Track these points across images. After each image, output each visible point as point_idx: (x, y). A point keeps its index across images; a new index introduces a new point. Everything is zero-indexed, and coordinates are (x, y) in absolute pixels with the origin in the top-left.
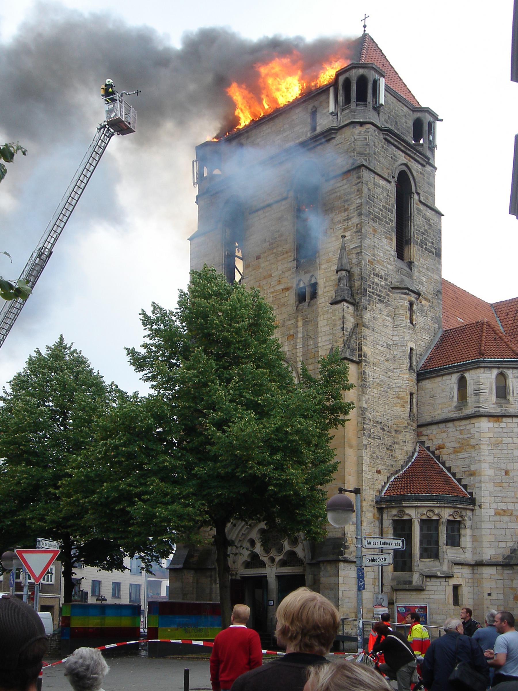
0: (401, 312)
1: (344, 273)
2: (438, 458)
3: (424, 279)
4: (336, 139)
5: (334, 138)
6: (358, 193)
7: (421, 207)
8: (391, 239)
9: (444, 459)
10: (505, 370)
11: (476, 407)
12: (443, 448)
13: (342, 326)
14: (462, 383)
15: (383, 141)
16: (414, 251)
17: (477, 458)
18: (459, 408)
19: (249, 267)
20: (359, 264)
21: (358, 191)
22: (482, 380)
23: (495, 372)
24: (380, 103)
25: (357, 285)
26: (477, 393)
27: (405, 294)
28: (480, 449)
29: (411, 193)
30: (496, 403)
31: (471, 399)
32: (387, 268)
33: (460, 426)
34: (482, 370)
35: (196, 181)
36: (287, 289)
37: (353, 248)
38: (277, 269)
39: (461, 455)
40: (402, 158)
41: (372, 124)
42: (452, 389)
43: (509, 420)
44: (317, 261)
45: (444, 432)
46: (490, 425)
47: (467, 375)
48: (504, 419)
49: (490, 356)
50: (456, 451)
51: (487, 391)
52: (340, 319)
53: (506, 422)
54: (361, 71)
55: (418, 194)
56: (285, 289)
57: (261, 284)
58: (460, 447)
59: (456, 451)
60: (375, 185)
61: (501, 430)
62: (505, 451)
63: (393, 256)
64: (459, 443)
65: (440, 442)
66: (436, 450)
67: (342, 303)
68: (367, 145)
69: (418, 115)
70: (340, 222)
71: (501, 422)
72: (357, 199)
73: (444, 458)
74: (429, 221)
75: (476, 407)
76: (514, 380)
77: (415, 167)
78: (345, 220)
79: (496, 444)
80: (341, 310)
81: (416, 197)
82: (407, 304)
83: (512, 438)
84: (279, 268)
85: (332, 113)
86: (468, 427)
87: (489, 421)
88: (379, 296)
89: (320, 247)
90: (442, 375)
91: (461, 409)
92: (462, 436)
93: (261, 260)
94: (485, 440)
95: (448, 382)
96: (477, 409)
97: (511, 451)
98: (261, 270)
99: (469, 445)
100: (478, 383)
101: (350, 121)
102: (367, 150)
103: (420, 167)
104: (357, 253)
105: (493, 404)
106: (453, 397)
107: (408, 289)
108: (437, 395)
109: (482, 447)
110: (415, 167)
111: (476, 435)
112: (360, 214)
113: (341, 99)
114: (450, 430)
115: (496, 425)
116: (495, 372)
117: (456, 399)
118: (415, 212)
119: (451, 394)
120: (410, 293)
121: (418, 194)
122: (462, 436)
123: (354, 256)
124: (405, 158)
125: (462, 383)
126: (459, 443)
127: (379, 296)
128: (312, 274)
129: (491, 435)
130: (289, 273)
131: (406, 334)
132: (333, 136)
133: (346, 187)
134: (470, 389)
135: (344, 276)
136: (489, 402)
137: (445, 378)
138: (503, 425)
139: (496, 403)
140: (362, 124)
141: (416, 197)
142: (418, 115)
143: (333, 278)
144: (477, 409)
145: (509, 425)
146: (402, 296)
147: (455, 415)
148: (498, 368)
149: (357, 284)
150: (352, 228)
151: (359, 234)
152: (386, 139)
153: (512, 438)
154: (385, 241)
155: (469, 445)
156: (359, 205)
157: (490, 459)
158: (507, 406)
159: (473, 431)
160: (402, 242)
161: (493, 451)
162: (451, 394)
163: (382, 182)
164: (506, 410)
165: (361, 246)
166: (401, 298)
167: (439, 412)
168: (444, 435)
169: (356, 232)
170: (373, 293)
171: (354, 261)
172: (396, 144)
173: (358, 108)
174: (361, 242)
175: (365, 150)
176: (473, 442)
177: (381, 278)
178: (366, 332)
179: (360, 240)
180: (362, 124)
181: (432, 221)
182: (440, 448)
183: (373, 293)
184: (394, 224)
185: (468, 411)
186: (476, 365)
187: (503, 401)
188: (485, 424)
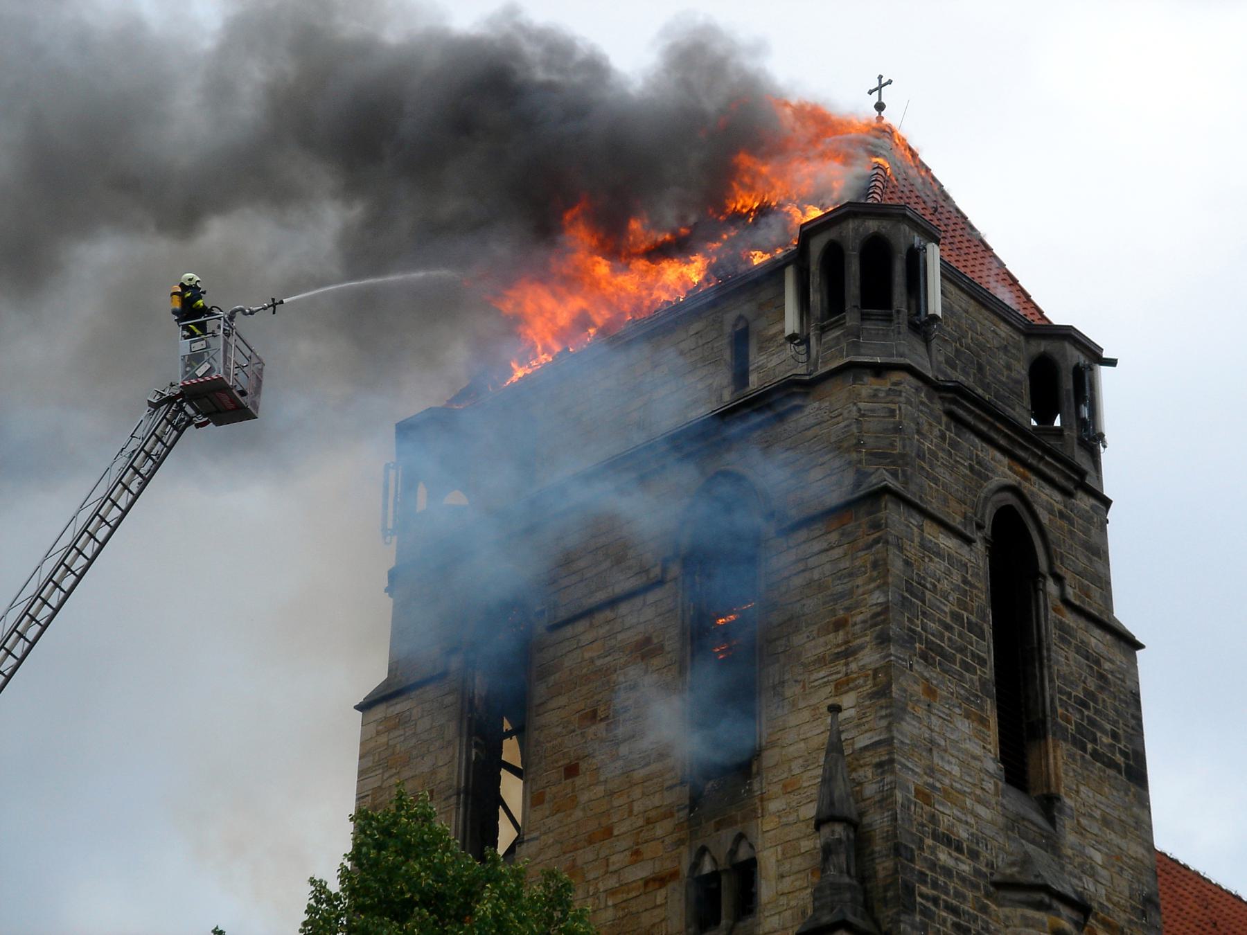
1: (839, 830)
3: (1098, 858)
4: (807, 411)
5: (798, 408)
6: (875, 574)
7: (1070, 619)
8: (983, 721)
15: (944, 419)
16: (1060, 761)
19: (542, 802)
21: (875, 565)
24: (930, 312)
25: (881, 874)
27: (1039, 906)
29: (1036, 575)
32: (976, 816)
35: (390, 525)
36: (661, 880)
37: (866, 748)
38: (631, 812)
40: (1003, 471)
44: (756, 786)
54: (872, 225)
55: (1059, 579)
56: (654, 880)
57: (579, 862)
63: (992, 776)
68: (897, 430)
69: (1043, 346)
70: (821, 661)
72: (871, 592)
74: (1098, 663)
77: (1044, 497)
78: (838, 656)
81: (1052, 587)
84: (637, 808)
88: (954, 911)
93: (579, 781)
98: (578, 814)
101: (846, 360)
102: (898, 444)
103: (1058, 496)
104: (880, 765)
107: (1046, 888)
110: (1044, 497)
118: (1054, 635)
120: (1056, 904)
121: (1059, 579)
123: (869, 772)
124: (1010, 469)
127: (954, 911)
128: (738, 828)
130: (668, 825)
133: (837, 553)
135: (840, 841)
140: (879, 370)
141: (1052, 587)
142: (1043, 346)
143: (806, 845)
149: (883, 867)
150: (861, 681)
151: (883, 701)
152: (950, 414)
156: (879, 609)
163: (947, 543)
165: (889, 742)
169: (872, 696)
170: (935, 901)
171: (870, 790)
175: (892, 445)
177: (959, 849)
179: (884, 723)
181: (1107, 666)
183: (935, 901)
184: (989, 672)
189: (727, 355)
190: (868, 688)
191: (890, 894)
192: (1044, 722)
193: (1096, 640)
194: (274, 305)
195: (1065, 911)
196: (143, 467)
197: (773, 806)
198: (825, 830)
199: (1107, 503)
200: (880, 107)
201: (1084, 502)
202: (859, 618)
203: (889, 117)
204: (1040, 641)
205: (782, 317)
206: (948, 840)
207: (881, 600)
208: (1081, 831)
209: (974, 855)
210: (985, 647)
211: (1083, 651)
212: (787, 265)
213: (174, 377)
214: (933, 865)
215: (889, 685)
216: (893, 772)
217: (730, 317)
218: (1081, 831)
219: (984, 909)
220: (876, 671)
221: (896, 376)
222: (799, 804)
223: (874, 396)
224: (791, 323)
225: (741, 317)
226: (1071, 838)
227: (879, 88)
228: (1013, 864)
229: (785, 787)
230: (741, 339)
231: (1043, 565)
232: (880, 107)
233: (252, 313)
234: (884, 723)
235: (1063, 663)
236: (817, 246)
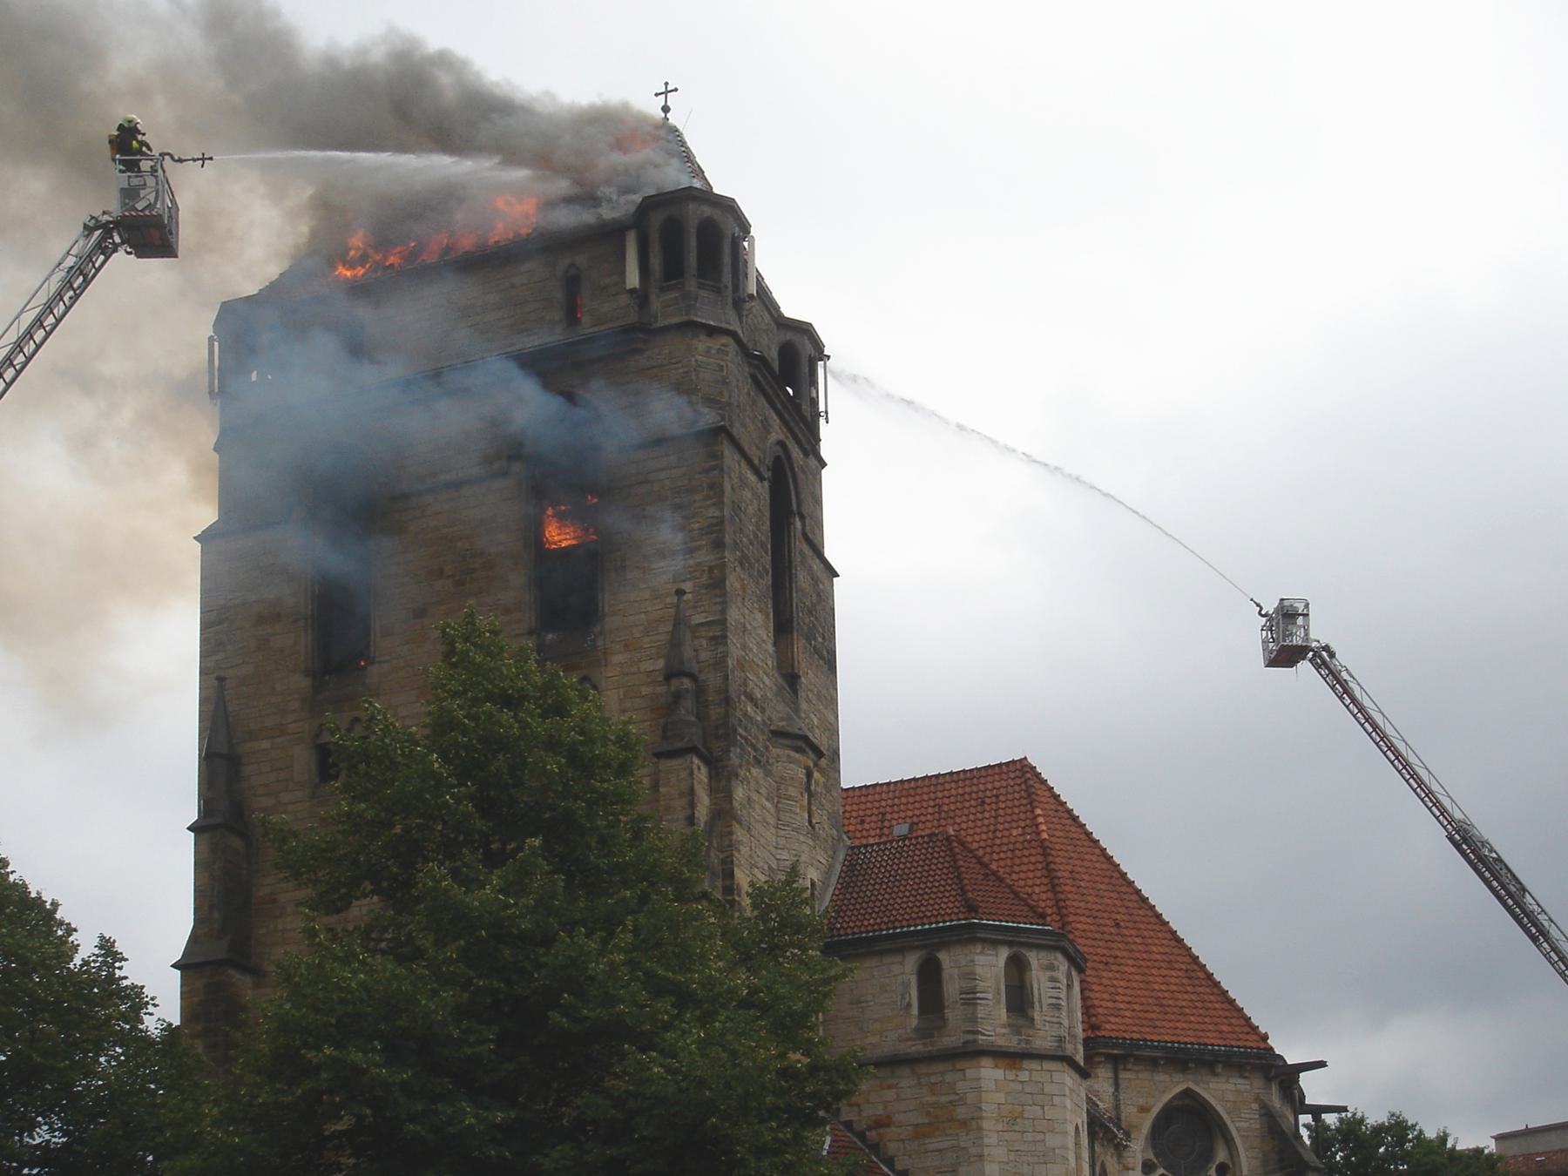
0: (792, 792)
2: (875, 1148)
5: (641, 351)
9: (891, 1152)
10: (1024, 951)
11: (968, 1032)
12: (888, 1126)
13: (689, 812)
14: (930, 976)
16: (800, 646)
17: (973, 1151)
18: (924, 1033)
20: (720, 664)
21: (711, 486)
22: (979, 970)
23: (1004, 953)
26: (970, 998)
27: (799, 750)
28: (980, 1129)
30: (1009, 1025)
31: (954, 1015)
33: (929, 1075)
34: (978, 948)
37: (702, 624)
39: (934, 1143)
41: (734, 335)
42: (906, 985)
43: (1035, 1065)
44: (600, 643)
45: (889, 1087)
46: (999, 1074)
47: (944, 957)
48: (1026, 1064)
49: (990, 915)
50: (919, 1133)
51: (990, 996)
52: (681, 795)
53: (1031, 1072)
58: (929, 1124)
59: (919, 1133)
60: (743, 482)
61: (1019, 1087)
62: (1028, 1137)
64: (928, 1113)
65: (880, 1111)
66: (870, 1129)
67: (688, 757)
68: (725, 382)
69: (789, 336)
71: (1020, 1069)
73: (892, 1148)
75: (968, 1032)
76: (1041, 974)
77: (796, 452)
79: (1013, 1119)
80: (683, 775)
82: (801, 773)
83: (1043, 1107)
85: (633, 291)
86: (949, 1077)
87: (996, 1067)
89: (606, 609)
90: (881, 953)
91: (931, 1035)
92: (934, 1098)
94: (989, 1109)
95: (896, 969)
96: (970, 1037)
97: (1040, 1136)
99: (952, 1120)
100: (970, 976)
101: (685, 318)
102: (726, 394)
104: (713, 638)
105: (1004, 1026)
106: (909, 1005)
107: (805, 738)
108: (870, 997)
109: (986, 1125)
111: (971, 1098)
112: (719, 545)
113: (656, 262)
114: (904, 1083)
115: (1011, 1075)
116: (1004, 953)
117: (915, 1010)
118: (797, 559)
119: (903, 997)
122: (934, 1098)
123: (704, 643)
125: (930, 976)
126: (928, 1113)
127: (755, 749)
129: (1001, 1098)
131: (804, 847)
132: (640, 346)
134: (952, 989)
136: (994, 1023)
137: (888, 960)
138: (1024, 1076)
139: (1009, 1025)
140: (712, 331)
142: (789, 336)
143: (645, 690)
144: (970, 1037)
145: (1037, 1077)
146: (793, 754)
147: (916, 1048)
148: (1010, 944)
149: (715, 712)
151: (717, 591)
152: (753, 377)
153: (1043, 1107)
154: (759, 616)
155: (952, 1120)
157: (1000, 1153)
158: (1030, 1032)
159: (961, 1086)
160: (783, 626)
161: (1006, 1136)
162: (903, 997)
164: (1028, 1042)
165: (723, 622)
166: (791, 760)
167: (875, 1039)
168: (890, 1095)
169: (707, 587)
170: (746, 739)
172: (770, 392)
173: (701, 292)
174: (723, 612)
175: (721, 393)
176: (961, 1113)
178: (739, 834)
179: (719, 608)
180: (712, 331)
182: (879, 1124)
185: (950, 1040)
186: (966, 935)
187: (1021, 1022)
188: (989, 1074)
189: (559, 295)
190: (704, 579)
191: (721, 732)
192: (792, 622)
193: (817, 566)
194: (203, 159)
195: (811, 754)
196: (78, 278)
197: (616, 659)
198: (675, 683)
199: (823, 464)
200: (666, 109)
201: (813, 462)
202: (696, 526)
203: (673, 118)
204: (790, 562)
205: (623, 273)
206: (751, 697)
207: (717, 514)
208: (809, 701)
209: (763, 711)
210: (767, 560)
211: (811, 572)
212: (628, 228)
213: (109, 205)
214: (745, 714)
215: (723, 580)
216: (726, 644)
217: (564, 262)
218: (809, 701)
219: (767, 748)
220: (711, 569)
221: (725, 340)
222: (640, 661)
223: (708, 352)
224: (633, 279)
225: (572, 265)
226: (804, 706)
227: (666, 93)
228: (782, 719)
229: (626, 645)
230: (572, 283)
231: (794, 507)
232: (666, 109)
233: (180, 161)
234: (719, 608)
235: (802, 578)
236: (656, 220)
